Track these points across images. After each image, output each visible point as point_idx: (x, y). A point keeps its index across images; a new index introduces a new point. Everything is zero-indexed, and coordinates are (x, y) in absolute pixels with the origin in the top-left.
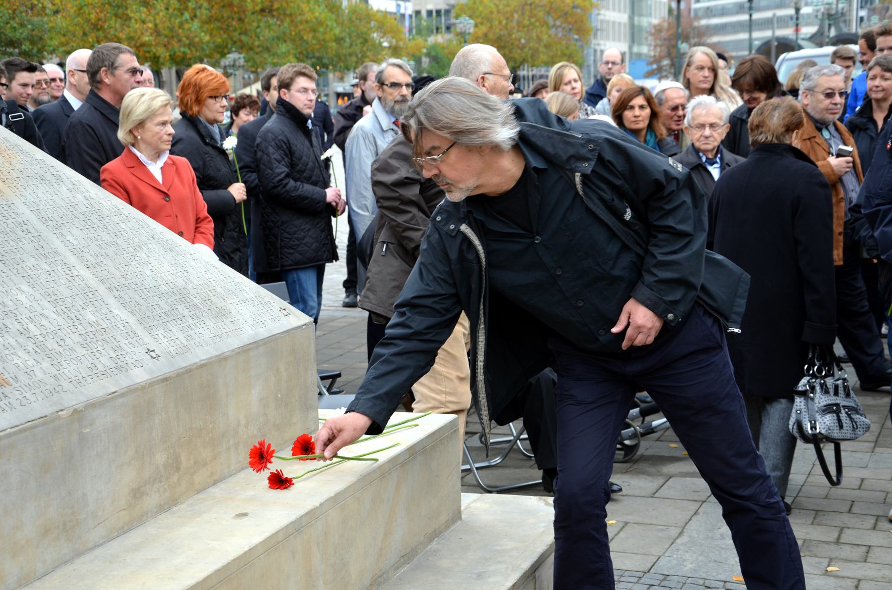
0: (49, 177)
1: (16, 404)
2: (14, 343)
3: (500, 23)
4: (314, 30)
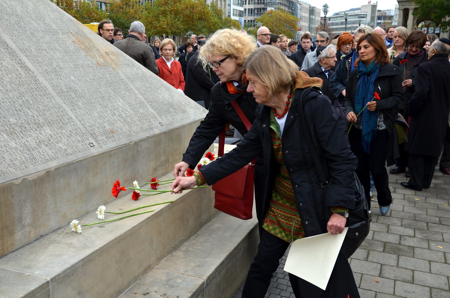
0: (131, 65)
1: (117, 139)
2: (117, 119)
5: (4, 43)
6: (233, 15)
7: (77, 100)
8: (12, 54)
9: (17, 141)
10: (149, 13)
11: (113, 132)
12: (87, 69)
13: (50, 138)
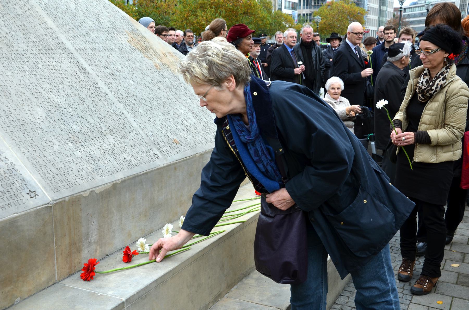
1: (181, 150)
2: (180, 128)
3: (330, 19)
4: (262, 20)
5: (61, 44)
6: (285, 7)
7: (137, 106)
8: (70, 56)
9: (82, 150)
10: (185, 7)
11: (177, 142)
12: (145, 72)
13: (114, 147)
